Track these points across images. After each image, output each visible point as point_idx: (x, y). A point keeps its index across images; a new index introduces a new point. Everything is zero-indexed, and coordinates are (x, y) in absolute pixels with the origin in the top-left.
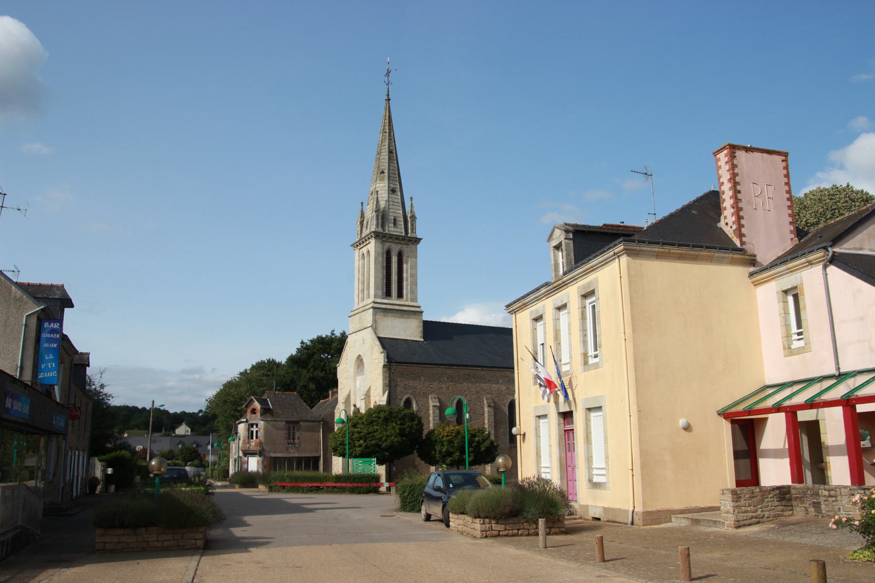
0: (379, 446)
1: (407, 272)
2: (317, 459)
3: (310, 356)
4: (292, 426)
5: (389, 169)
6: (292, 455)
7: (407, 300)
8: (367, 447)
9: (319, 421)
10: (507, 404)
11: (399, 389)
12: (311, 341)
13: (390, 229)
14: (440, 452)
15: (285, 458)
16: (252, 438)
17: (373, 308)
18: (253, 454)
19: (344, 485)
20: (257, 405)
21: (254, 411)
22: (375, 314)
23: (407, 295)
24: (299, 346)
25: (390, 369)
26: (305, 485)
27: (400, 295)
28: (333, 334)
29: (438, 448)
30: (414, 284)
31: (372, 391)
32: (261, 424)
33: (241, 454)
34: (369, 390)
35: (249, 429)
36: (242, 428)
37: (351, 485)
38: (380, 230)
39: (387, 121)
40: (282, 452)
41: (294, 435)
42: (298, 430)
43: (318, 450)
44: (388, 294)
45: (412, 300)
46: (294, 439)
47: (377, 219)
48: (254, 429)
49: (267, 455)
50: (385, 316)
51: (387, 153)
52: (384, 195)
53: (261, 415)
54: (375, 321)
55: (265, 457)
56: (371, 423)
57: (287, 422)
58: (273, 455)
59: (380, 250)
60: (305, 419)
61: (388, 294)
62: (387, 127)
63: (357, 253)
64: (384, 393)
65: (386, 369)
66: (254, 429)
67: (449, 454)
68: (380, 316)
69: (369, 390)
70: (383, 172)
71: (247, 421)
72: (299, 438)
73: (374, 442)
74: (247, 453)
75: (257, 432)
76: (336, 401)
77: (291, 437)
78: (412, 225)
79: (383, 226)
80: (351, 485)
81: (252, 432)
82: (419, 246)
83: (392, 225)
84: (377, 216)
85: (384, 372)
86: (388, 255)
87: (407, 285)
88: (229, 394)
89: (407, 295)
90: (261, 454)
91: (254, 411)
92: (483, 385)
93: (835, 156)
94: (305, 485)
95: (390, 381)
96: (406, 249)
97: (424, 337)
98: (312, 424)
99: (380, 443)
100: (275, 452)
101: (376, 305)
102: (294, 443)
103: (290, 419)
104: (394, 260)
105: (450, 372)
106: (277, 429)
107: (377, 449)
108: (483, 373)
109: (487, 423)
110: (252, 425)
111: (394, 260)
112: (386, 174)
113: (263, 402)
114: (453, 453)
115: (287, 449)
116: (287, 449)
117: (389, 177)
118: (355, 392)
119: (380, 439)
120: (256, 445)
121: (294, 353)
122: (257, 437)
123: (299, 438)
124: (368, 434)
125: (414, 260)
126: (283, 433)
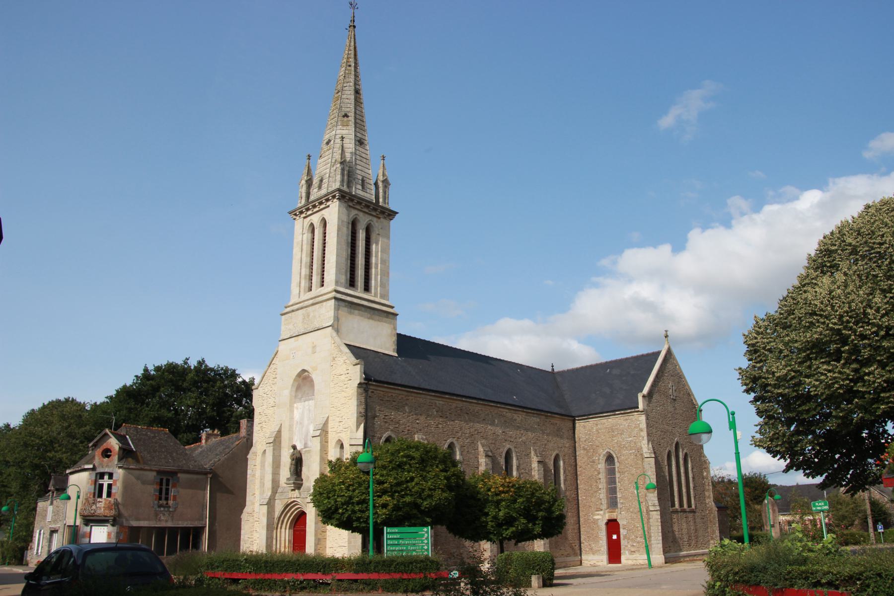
0: (416, 506)
1: (377, 256)
2: (198, 531)
3: (155, 389)
4: (166, 481)
5: (355, 113)
6: (163, 524)
7: (376, 296)
8: (397, 508)
9: (206, 474)
10: (504, 455)
11: (378, 422)
12: (158, 369)
13: (357, 190)
14: (495, 518)
15: (150, 529)
16: (100, 496)
17: (335, 298)
18: (101, 521)
19: (373, 576)
20: (114, 443)
21: (107, 453)
22: (337, 309)
23: (376, 289)
24: (140, 372)
25: (366, 391)
26: (289, 577)
27: (367, 288)
28: (186, 363)
29: (491, 510)
30: (385, 273)
31: (330, 425)
32: (119, 473)
33: (79, 522)
34: (326, 423)
35: (96, 481)
36: (79, 481)
37: (387, 577)
38: (345, 188)
39: (352, 52)
40: (148, 519)
41: (167, 493)
42: (174, 486)
43: (202, 518)
44: (352, 283)
45: (382, 297)
46: (167, 499)
47: (343, 174)
48: (106, 482)
49: (125, 524)
50: (350, 313)
51: (353, 92)
52: (350, 145)
53: (120, 460)
54: (337, 319)
55: (122, 526)
56: (400, 466)
57: (159, 472)
58: (135, 524)
59: (345, 218)
60: (185, 468)
61: (352, 283)
62: (352, 60)
63: (300, 225)
64: (358, 427)
65: (361, 390)
66: (106, 482)
67: (509, 521)
68: (344, 312)
69: (326, 423)
70: (346, 116)
71: (94, 469)
72: (175, 498)
73: (408, 499)
74: (91, 520)
75: (110, 486)
76: (248, 443)
77: (163, 494)
78: (385, 192)
79: (349, 186)
80: (387, 577)
81: (101, 486)
82: (393, 223)
83: (360, 187)
84: (343, 170)
85: (359, 394)
86: (354, 224)
87: (376, 275)
88: (32, 434)
89: (376, 289)
90: (115, 521)
91: (107, 453)
92: (478, 426)
93: (605, 262)
94: (289, 577)
95: (366, 410)
96: (377, 224)
97: (398, 351)
98: (195, 477)
99: (419, 501)
100: (138, 519)
101: (339, 296)
102: (167, 506)
103: (163, 468)
104: (361, 235)
105: (440, 402)
106: (144, 483)
107: (415, 511)
108: (478, 408)
109: (536, 474)
110: (101, 475)
111: (361, 235)
112: (352, 118)
113: (121, 439)
114: (515, 519)
115: (156, 515)
116: (156, 515)
117: (356, 123)
118: (291, 427)
119: (420, 494)
120: (109, 508)
121: (129, 383)
122: (109, 494)
123: (175, 498)
124: (399, 484)
125: (385, 240)
126: (152, 489)
